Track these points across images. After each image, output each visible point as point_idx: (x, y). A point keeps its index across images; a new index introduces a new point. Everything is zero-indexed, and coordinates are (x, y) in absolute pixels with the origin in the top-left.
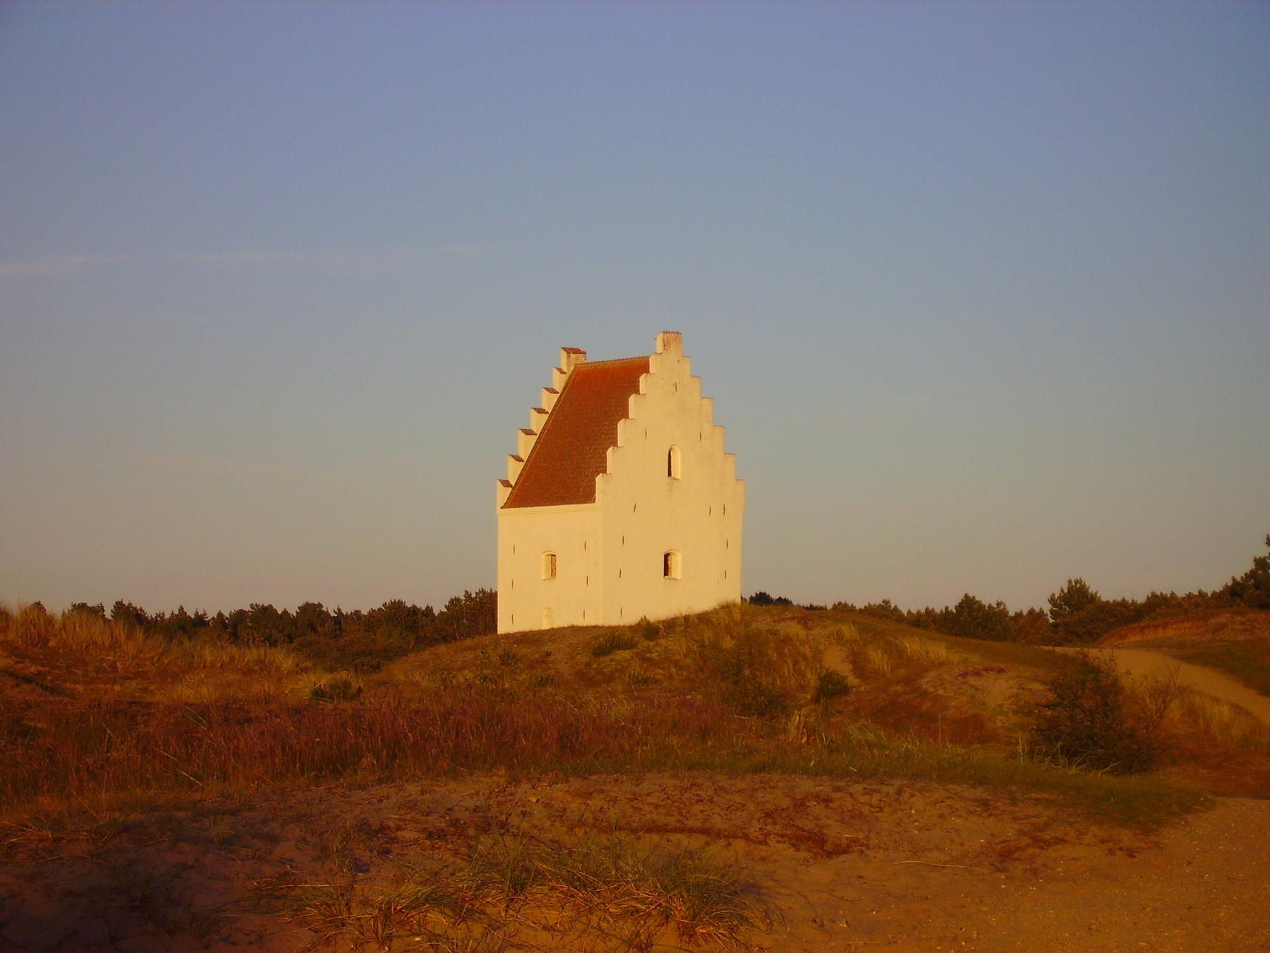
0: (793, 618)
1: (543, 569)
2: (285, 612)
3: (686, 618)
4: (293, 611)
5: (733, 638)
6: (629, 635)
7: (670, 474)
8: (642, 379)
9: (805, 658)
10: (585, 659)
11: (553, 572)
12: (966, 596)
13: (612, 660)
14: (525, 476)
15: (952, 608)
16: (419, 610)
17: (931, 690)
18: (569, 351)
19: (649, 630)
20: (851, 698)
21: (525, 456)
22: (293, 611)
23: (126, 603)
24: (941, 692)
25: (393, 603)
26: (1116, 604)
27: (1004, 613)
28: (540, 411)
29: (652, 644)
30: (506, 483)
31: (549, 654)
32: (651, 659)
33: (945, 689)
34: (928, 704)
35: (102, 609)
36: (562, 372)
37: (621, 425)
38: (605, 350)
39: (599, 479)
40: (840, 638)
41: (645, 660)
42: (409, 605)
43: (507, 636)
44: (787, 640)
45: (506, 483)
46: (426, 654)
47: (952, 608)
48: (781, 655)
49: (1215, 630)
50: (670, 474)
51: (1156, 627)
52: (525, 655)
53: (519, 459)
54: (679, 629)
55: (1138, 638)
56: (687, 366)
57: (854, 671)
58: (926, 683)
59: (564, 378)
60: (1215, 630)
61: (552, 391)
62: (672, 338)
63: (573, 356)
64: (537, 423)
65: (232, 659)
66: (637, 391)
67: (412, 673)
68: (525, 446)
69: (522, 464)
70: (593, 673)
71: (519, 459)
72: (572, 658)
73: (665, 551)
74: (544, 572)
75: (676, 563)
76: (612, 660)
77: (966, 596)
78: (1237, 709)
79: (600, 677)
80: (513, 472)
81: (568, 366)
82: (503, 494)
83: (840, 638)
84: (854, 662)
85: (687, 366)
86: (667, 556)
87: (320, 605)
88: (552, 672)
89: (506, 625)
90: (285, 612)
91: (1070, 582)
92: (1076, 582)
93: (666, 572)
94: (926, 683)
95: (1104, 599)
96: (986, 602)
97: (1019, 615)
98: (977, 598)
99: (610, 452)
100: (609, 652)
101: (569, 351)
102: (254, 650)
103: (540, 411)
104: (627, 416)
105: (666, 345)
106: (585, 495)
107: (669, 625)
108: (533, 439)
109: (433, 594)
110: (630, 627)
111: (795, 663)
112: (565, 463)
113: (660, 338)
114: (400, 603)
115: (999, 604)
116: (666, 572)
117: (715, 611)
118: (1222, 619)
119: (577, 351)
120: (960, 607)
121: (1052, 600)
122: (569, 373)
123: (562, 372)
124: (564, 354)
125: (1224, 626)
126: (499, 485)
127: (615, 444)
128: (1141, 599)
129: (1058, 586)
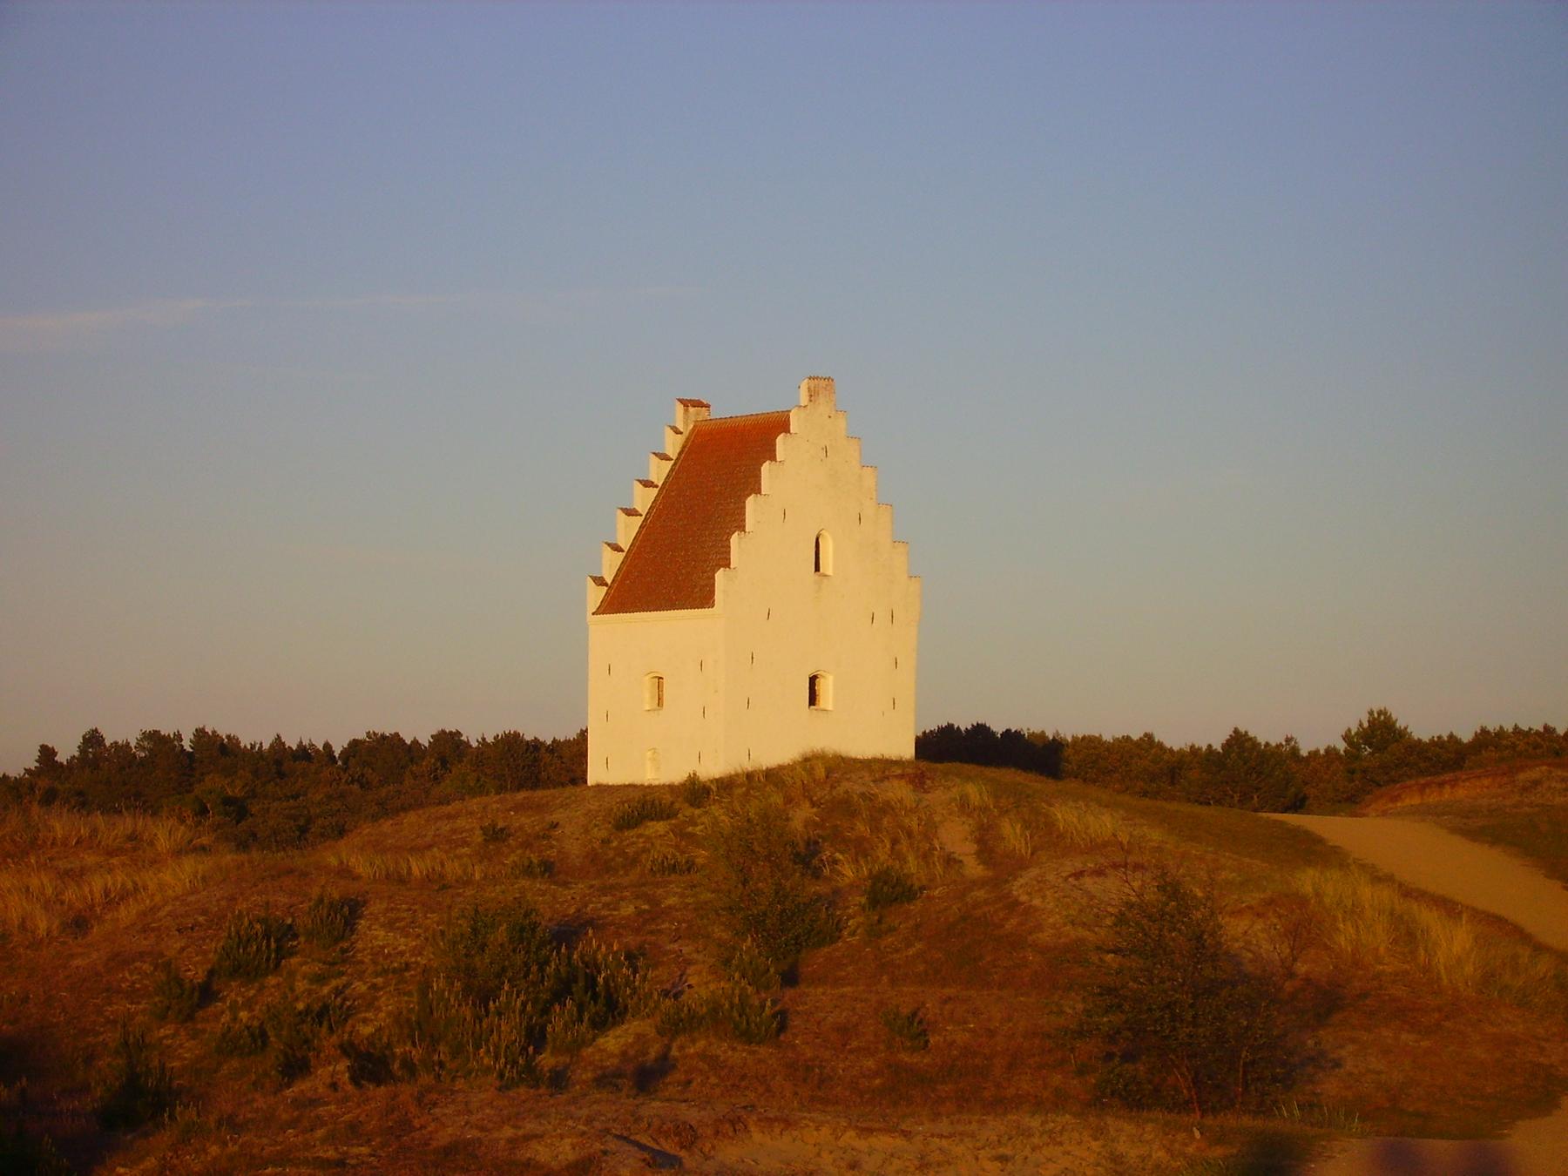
0: (902, 776)
1: (647, 696)
2: (415, 742)
3: (749, 776)
4: (425, 741)
5: (813, 805)
6: (668, 798)
7: (817, 569)
8: (780, 440)
9: (910, 835)
10: (604, 834)
11: (813, 680)
12: (1236, 731)
13: (640, 836)
14: (624, 574)
15: (1217, 747)
16: (543, 744)
17: (1024, 898)
18: (686, 403)
19: (695, 792)
20: (916, 907)
21: (625, 545)
22: (425, 741)
23: (209, 730)
24: (1037, 902)
25: (507, 736)
26: (1437, 743)
27: (1295, 751)
28: (647, 484)
29: (697, 812)
30: (599, 581)
31: (555, 826)
32: (693, 835)
33: (1044, 897)
34: (1013, 922)
35: (179, 737)
36: (678, 432)
37: (751, 502)
38: (733, 403)
39: (720, 575)
40: (964, 806)
41: (683, 835)
42: (528, 737)
43: (600, 788)
44: (887, 809)
45: (599, 581)
46: (386, 826)
47: (1217, 747)
48: (876, 829)
49: (1525, 789)
50: (817, 569)
51: (1441, 785)
52: (521, 828)
53: (617, 549)
54: (739, 791)
55: (1416, 801)
56: (841, 423)
57: (979, 854)
58: (1019, 888)
59: (680, 439)
60: (1525, 789)
61: (664, 457)
62: (821, 385)
63: (691, 409)
64: (643, 500)
65: (95, 831)
66: (772, 457)
67: (439, 841)
68: (626, 531)
69: (621, 556)
70: (611, 854)
71: (617, 549)
72: (587, 831)
73: (811, 672)
74: (648, 702)
75: (826, 688)
76: (640, 836)
77: (1236, 731)
78: (1494, 924)
79: (620, 860)
80: (610, 565)
81: (686, 424)
82: (596, 595)
83: (964, 806)
84: (980, 841)
85: (841, 423)
86: (813, 680)
87: (458, 733)
88: (554, 853)
89: (597, 773)
90: (415, 742)
91: (1371, 713)
92: (1380, 713)
93: (813, 700)
94: (1019, 888)
95: (1416, 736)
96: (1262, 740)
97: (1314, 755)
98: (1251, 734)
99: (734, 539)
100: (636, 826)
101: (686, 403)
102: (129, 821)
103: (647, 484)
104: (758, 491)
105: (812, 395)
106: (704, 598)
107: (726, 785)
108: (638, 521)
109: (544, 728)
110: (671, 788)
111: (895, 842)
112: (674, 558)
113: (804, 385)
114: (516, 735)
115: (1288, 740)
116: (813, 700)
117: (791, 768)
118: (1535, 774)
119: (698, 404)
120: (1228, 745)
121: (1347, 737)
122: (686, 434)
123: (678, 432)
124: (680, 408)
125: (1536, 783)
126: (590, 582)
127: (742, 528)
128: (1466, 736)
129: (1355, 718)
